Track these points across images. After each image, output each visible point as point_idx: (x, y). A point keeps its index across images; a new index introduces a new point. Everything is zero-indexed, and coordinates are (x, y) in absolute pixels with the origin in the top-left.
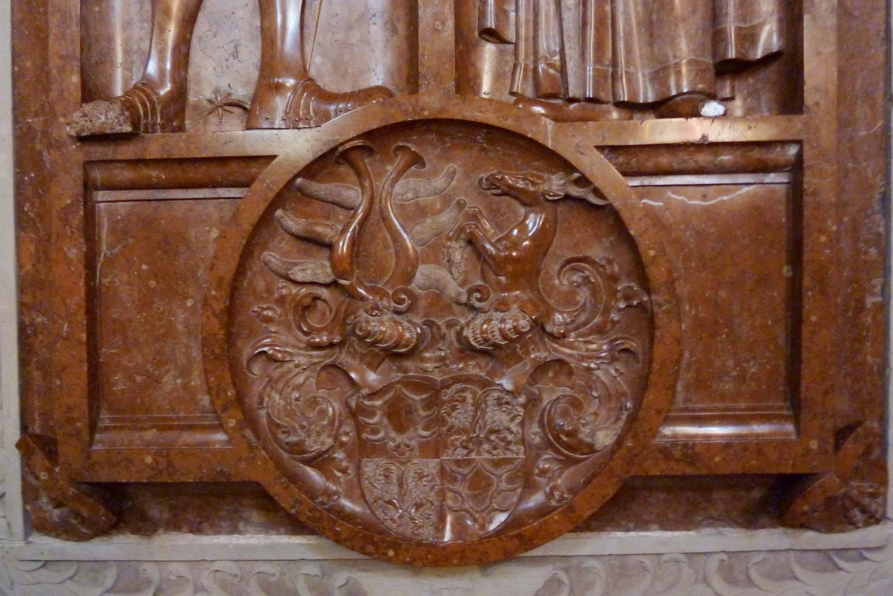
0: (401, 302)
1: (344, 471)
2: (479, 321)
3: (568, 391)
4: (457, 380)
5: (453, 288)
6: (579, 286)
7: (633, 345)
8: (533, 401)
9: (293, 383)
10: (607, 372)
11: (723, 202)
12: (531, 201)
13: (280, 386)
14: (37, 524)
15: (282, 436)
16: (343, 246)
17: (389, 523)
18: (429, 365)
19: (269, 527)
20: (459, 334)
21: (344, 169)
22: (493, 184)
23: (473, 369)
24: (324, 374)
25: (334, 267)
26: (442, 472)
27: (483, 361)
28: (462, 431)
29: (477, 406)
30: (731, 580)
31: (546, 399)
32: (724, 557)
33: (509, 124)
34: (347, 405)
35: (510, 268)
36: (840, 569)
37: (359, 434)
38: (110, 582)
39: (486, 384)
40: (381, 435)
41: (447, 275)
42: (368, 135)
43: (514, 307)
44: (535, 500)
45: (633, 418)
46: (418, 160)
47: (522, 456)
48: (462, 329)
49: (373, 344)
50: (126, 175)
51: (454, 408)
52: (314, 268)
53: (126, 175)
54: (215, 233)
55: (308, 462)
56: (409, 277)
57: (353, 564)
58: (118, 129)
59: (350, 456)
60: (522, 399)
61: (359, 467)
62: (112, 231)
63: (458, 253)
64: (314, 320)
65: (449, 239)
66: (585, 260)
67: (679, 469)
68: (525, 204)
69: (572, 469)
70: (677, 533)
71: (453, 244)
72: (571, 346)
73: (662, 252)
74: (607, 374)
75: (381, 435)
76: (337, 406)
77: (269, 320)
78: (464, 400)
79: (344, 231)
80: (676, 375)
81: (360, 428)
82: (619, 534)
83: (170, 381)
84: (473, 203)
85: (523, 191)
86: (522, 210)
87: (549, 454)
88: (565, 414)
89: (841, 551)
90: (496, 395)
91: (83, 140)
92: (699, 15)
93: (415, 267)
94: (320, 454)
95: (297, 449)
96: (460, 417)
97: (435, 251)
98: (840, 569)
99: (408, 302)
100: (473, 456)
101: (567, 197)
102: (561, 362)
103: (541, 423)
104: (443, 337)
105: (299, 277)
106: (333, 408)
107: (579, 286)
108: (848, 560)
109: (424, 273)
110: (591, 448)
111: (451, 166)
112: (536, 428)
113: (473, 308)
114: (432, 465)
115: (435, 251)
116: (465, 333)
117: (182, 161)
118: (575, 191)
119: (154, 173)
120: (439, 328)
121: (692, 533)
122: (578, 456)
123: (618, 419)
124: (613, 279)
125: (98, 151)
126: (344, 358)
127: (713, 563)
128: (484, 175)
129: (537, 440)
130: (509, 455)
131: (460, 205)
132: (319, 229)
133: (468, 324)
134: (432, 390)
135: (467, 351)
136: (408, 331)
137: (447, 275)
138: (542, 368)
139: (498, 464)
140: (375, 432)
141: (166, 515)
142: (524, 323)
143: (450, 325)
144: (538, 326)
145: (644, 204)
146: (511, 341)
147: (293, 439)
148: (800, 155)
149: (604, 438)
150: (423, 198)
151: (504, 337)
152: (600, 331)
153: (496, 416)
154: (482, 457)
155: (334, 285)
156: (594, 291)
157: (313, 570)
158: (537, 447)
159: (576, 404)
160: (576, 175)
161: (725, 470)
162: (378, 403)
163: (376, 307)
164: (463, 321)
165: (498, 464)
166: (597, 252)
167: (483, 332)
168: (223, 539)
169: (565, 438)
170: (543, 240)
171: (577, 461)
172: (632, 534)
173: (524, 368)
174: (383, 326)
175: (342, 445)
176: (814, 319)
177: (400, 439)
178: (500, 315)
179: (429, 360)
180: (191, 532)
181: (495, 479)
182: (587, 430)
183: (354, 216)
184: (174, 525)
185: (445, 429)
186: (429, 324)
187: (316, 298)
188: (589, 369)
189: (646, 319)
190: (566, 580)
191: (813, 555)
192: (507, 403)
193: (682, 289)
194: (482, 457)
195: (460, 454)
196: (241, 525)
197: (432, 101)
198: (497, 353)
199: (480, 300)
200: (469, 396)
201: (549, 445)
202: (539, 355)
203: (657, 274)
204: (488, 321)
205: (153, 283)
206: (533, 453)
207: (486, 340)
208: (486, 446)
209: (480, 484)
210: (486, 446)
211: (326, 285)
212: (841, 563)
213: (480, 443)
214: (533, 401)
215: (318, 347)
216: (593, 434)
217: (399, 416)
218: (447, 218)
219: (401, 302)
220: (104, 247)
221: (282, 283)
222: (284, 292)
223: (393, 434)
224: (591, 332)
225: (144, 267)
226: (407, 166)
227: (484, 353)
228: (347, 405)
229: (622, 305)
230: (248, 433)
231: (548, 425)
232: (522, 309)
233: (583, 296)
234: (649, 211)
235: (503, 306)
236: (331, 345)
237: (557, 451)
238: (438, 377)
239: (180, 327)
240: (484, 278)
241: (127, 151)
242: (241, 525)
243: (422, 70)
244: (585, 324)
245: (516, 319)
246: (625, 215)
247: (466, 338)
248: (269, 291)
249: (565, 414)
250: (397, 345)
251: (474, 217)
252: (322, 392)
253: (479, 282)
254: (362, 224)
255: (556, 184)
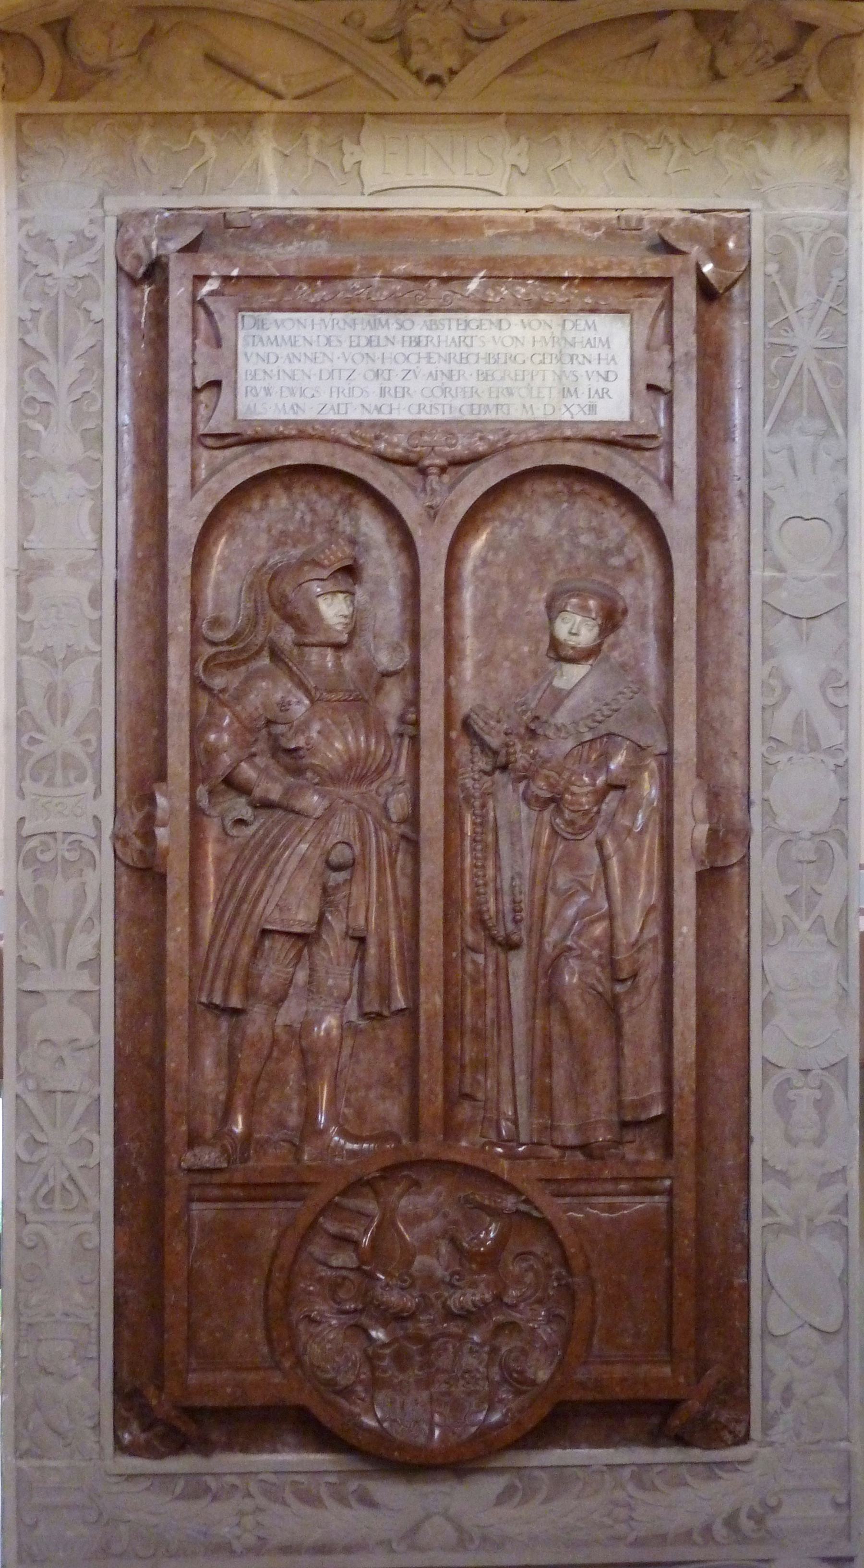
0: (405, 1281)
1: (363, 1400)
2: (457, 1295)
3: (519, 1344)
4: (443, 1335)
5: (440, 1272)
6: (526, 1271)
7: (563, 1312)
8: (494, 1350)
9: (326, 1336)
10: (545, 1331)
11: (623, 1215)
12: (495, 1213)
13: (318, 1339)
14: (120, 1447)
15: (319, 1373)
16: (366, 1241)
17: (394, 1435)
18: (423, 1325)
19: (301, 1446)
20: (444, 1304)
21: (366, 1190)
22: (467, 1200)
23: (454, 1328)
24: (349, 1332)
25: (358, 1256)
26: (431, 1400)
27: (460, 1323)
28: (445, 1371)
29: (456, 1354)
30: (641, 1485)
31: (504, 1350)
32: (635, 1468)
33: (480, 1164)
34: (365, 1351)
35: (479, 1259)
36: (720, 1478)
37: (373, 1373)
38: (178, 1490)
39: (462, 1338)
40: (388, 1375)
41: (435, 1263)
42: (384, 1169)
43: (482, 1285)
44: (496, 1417)
45: (560, 1363)
46: (417, 1184)
47: (487, 1388)
48: (446, 1300)
49: (386, 1310)
50: (216, 1192)
51: (440, 1356)
52: (344, 1259)
53: (216, 1192)
54: (274, 1233)
55: (339, 1393)
56: (411, 1263)
57: (362, 1474)
58: (218, 1165)
59: (366, 1391)
60: (486, 1349)
61: (372, 1397)
62: (202, 1230)
63: (444, 1248)
64: (342, 1294)
65: (438, 1238)
66: (531, 1253)
67: (590, 1396)
68: (489, 1215)
69: (522, 1398)
70: (600, 1451)
71: (440, 1241)
72: (521, 1313)
73: (581, 1248)
74: (546, 1333)
75: (388, 1375)
76: (357, 1354)
77: (310, 1293)
78: (446, 1350)
79: (366, 1232)
80: (592, 1333)
81: (373, 1369)
82: (559, 1451)
83: (241, 1336)
84: (455, 1214)
85: (489, 1207)
86: (488, 1219)
87: (505, 1387)
88: (516, 1360)
89: (722, 1464)
90: (469, 1345)
91: (189, 1170)
92: (608, 1089)
93: (414, 1256)
94: (346, 1388)
95: (331, 1384)
96: (444, 1362)
97: (428, 1246)
98: (720, 1478)
99: (409, 1281)
100: (453, 1389)
101: (518, 1212)
102: (513, 1323)
103: (501, 1368)
104: (432, 1305)
105: (334, 1263)
106: (357, 1354)
107: (526, 1271)
108: (727, 1471)
109: (420, 1261)
110: (533, 1383)
111: (440, 1188)
112: (496, 1369)
113: (453, 1286)
114: (424, 1395)
115: (428, 1246)
116: (448, 1303)
117: (257, 1185)
118: (523, 1207)
119: (235, 1192)
120: (429, 1299)
121: (611, 1450)
122: (524, 1388)
123: (551, 1364)
124: (549, 1266)
125: (200, 1178)
126: (364, 1320)
127: (627, 1472)
128: (462, 1194)
129: (497, 1378)
130: (478, 1388)
131: (445, 1215)
132: (348, 1231)
133: (450, 1296)
134: (426, 1344)
135: (450, 1315)
136: (410, 1301)
137: (435, 1263)
138: (500, 1328)
139: (469, 1394)
140: (385, 1371)
141: (224, 1439)
142: (488, 1296)
143: (438, 1297)
144: (498, 1298)
145: (569, 1217)
146: (479, 1308)
147: (328, 1376)
148: (671, 1186)
149: (543, 1375)
150: (422, 1209)
151: (475, 1305)
152: (540, 1301)
153: (469, 1361)
154: (459, 1390)
155: (358, 1269)
156: (536, 1273)
157: (332, 1479)
158: (498, 1383)
159: (524, 1352)
160: (523, 1197)
161: (622, 1397)
162: (387, 1351)
163: (387, 1285)
164: (446, 1294)
165: (469, 1394)
166: (538, 1249)
167: (460, 1302)
168: (265, 1457)
169: (515, 1375)
170: (501, 1241)
171: (525, 1392)
172: (568, 1451)
173: (487, 1328)
174: (393, 1298)
175: (361, 1382)
176: (680, 1295)
177: (401, 1377)
178: (472, 1291)
179: (422, 1322)
180: (241, 1451)
181: (467, 1404)
182: (532, 1370)
183: (372, 1221)
184: (229, 1447)
185: (433, 1370)
186: (423, 1296)
187: (344, 1278)
188: (533, 1329)
189: (569, 1293)
190: (519, 1485)
191: (701, 1468)
192: (477, 1352)
193: (595, 1273)
194: (459, 1390)
195: (444, 1388)
196: (279, 1446)
197: (426, 1148)
198: (469, 1317)
199: (458, 1280)
200: (450, 1347)
201: (504, 1380)
202: (498, 1318)
203: (577, 1263)
204: (464, 1295)
205: (229, 1268)
206: (495, 1387)
207: (462, 1308)
208: (462, 1382)
209: (457, 1407)
210: (462, 1382)
211: (352, 1269)
212: (720, 1473)
213: (458, 1380)
214: (494, 1350)
215: (347, 1312)
216: (535, 1373)
217: (401, 1360)
218: (436, 1224)
219: (405, 1281)
220: (195, 1241)
221: (320, 1267)
222: (323, 1274)
223: (397, 1374)
224: (533, 1303)
225: (224, 1256)
226: (410, 1187)
227: (460, 1316)
228: (365, 1351)
229: (555, 1284)
230: (299, 1371)
231: (504, 1367)
232: (487, 1286)
233: (529, 1277)
234: (572, 1221)
235: (474, 1285)
236: (355, 1311)
237: (511, 1385)
238: (429, 1334)
239: (248, 1298)
240: (461, 1265)
241: (218, 1179)
242: (279, 1446)
243: (421, 1127)
244: (530, 1297)
245: (481, 1294)
246: (556, 1225)
247: (449, 1307)
248: (312, 1273)
249: (516, 1360)
250: (402, 1311)
251: (455, 1223)
252: (347, 1344)
253: (458, 1268)
254: (377, 1227)
255: (510, 1202)
